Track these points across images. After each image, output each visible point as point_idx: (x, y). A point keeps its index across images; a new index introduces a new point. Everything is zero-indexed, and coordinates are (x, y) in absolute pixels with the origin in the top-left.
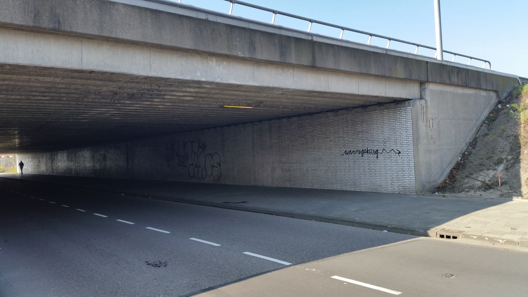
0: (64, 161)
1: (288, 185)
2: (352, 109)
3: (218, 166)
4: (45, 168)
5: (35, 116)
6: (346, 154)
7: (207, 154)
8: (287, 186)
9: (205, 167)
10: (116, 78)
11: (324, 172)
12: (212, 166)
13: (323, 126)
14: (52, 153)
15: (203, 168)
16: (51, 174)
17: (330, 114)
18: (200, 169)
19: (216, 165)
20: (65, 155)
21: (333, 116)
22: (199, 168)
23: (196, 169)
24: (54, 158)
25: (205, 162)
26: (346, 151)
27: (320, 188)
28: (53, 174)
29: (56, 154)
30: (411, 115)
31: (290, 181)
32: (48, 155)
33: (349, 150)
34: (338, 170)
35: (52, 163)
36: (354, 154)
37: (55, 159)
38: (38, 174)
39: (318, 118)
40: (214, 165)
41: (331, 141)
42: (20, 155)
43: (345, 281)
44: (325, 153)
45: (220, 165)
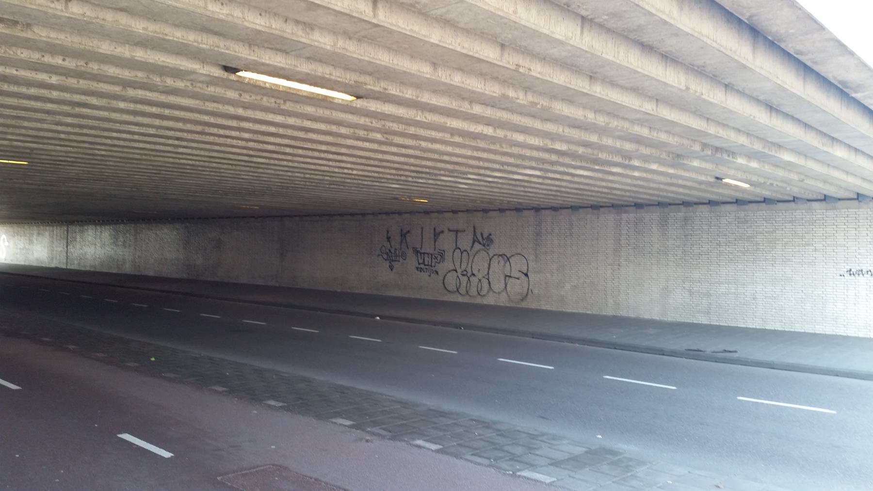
0: (103, 245)
1: (703, 320)
2: (870, 201)
3: (523, 277)
4: (46, 255)
5: (118, 173)
6: (850, 275)
7: (495, 255)
8: (700, 322)
9: (487, 277)
10: (183, 39)
11: (794, 302)
12: (506, 276)
13: (800, 224)
14: (69, 229)
15: (484, 277)
16: (64, 267)
17: (815, 205)
18: (474, 280)
19: (515, 273)
20: (47, 234)
21: (824, 209)
22: (472, 279)
23: (464, 280)
24: (75, 239)
25: (489, 269)
26: (850, 270)
27: (783, 329)
28: (68, 267)
29: (87, 230)
30: (422, 255)
31: (708, 313)
32: (58, 231)
33: (858, 268)
34: (830, 301)
35: (67, 247)
36: (868, 276)
37: (78, 240)
38: (27, 263)
39: (788, 210)
40: (512, 275)
41: (816, 250)
42: (15, 226)
43: (328, 95)
44: (801, 271)
45: (526, 275)
